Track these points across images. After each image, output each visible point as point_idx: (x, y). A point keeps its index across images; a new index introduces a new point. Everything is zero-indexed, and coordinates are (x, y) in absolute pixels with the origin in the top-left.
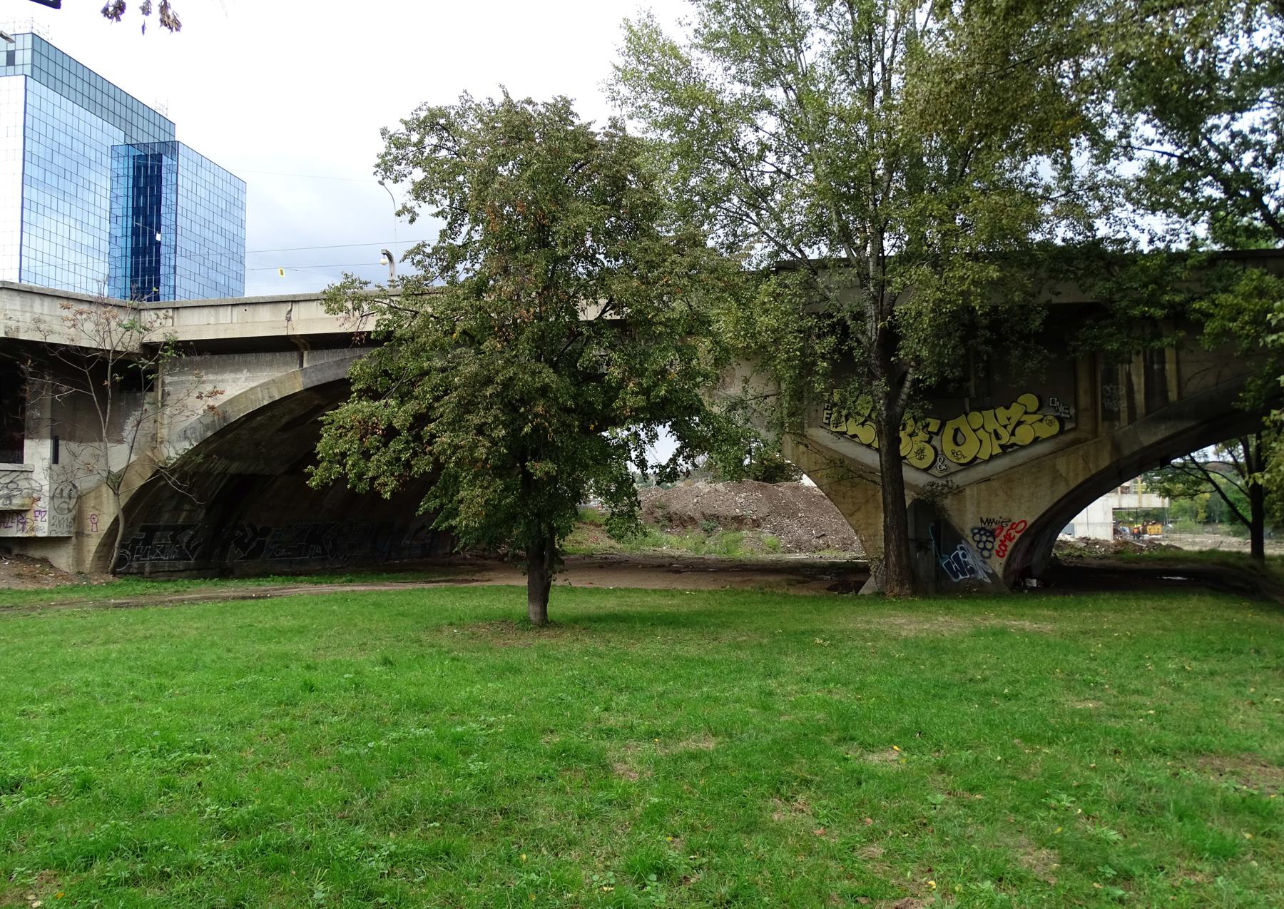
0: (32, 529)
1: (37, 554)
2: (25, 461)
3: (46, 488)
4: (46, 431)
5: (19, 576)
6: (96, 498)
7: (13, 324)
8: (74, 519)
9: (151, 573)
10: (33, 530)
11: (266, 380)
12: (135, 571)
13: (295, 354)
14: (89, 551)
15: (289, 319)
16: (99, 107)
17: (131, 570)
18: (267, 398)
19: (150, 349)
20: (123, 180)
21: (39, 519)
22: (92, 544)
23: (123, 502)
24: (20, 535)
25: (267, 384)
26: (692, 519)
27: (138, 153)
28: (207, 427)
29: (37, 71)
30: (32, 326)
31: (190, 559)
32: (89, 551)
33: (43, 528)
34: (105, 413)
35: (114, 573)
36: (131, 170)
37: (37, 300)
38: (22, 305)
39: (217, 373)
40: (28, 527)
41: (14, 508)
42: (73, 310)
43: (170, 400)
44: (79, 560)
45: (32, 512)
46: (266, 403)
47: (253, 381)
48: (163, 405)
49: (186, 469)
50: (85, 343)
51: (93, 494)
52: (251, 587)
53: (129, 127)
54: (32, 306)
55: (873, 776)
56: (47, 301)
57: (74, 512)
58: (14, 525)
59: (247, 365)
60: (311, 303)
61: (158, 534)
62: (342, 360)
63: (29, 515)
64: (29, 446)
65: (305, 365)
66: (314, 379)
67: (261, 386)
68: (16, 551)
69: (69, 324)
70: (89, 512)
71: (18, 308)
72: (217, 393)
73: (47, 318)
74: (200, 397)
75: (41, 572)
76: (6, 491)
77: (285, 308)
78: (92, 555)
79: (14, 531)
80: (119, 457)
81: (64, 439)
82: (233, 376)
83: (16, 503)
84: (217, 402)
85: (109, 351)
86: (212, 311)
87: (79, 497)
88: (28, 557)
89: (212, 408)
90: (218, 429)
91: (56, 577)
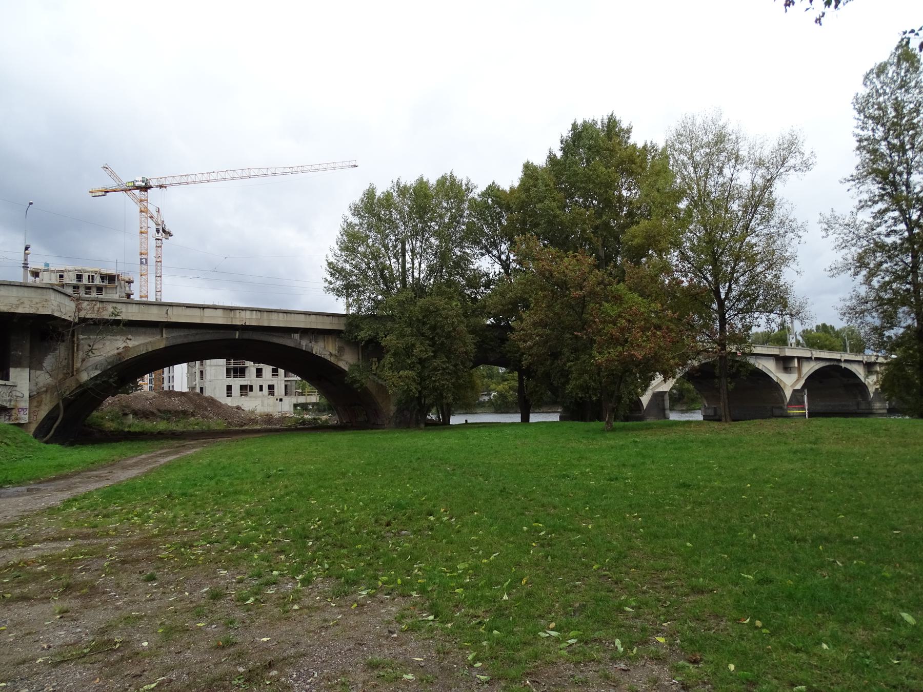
0: (17, 419)
15: (167, 313)
22: (33, 427)
25: (147, 343)
26: (153, 414)
28: (109, 363)
40: (13, 418)
63: (14, 411)
65: (164, 335)
77: (165, 308)
86: (137, 306)
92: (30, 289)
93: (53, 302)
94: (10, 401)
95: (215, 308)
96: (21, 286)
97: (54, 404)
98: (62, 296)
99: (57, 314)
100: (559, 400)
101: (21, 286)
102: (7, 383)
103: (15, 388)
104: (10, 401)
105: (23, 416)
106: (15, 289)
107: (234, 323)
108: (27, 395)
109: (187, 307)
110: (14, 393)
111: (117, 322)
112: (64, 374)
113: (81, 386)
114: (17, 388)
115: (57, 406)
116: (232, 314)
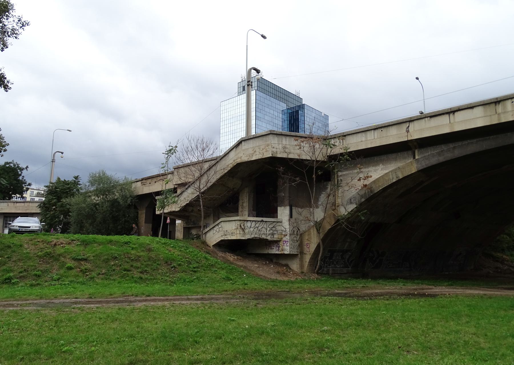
1: (284, 262)
3: (288, 230)
4: (287, 202)
5: (278, 272)
6: (308, 235)
7: (275, 150)
8: (299, 246)
9: (332, 274)
10: (283, 250)
11: (393, 168)
12: (326, 273)
13: (410, 152)
15: (408, 131)
16: (278, 97)
17: (324, 272)
18: (395, 178)
19: (333, 158)
20: (286, 122)
21: (285, 245)
22: (307, 258)
23: (322, 236)
24: (277, 252)
25: (396, 170)
27: (291, 111)
28: (362, 196)
29: (259, 88)
30: (282, 151)
31: (349, 268)
32: (306, 262)
33: (287, 249)
34: (312, 193)
35: (318, 273)
36: (288, 118)
37: (284, 138)
41: (275, 240)
42: (299, 141)
43: (343, 184)
44: (302, 266)
46: (394, 181)
47: (386, 170)
48: (338, 187)
49: (350, 219)
50: (304, 157)
51: (307, 233)
52: (410, 287)
53: (287, 103)
54: (282, 141)
55: (142, 256)
56: (288, 138)
57: (299, 242)
58: (275, 248)
59: (382, 162)
60: (421, 120)
61: (335, 254)
62: (442, 151)
63: (281, 243)
64: (280, 210)
65: (417, 157)
66: (424, 164)
67: (391, 171)
68: (274, 261)
69: (298, 147)
70: (306, 242)
71: (277, 142)
72: (368, 177)
73: (288, 146)
74: (359, 180)
75: (287, 271)
76: (271, 231)
78: (307, 263)
79: (274, 251)
80: (319, 214)
81: (294, 206)
82: (374, 168)
83: (276, 237)
84: (367, 182)
85: (314, 161)
86: (363, 134)
87: (301, 235)
88: (280, 264)
89: (365, 186)
90: (368, 197)
91: (293, 274)
94: (273, 234)
95: (471, 107)
98: (355, 136)
100: (251, 84)
103: (280, 224)
107: (503, 120)
109: (431, 117)
116: (500, 108)
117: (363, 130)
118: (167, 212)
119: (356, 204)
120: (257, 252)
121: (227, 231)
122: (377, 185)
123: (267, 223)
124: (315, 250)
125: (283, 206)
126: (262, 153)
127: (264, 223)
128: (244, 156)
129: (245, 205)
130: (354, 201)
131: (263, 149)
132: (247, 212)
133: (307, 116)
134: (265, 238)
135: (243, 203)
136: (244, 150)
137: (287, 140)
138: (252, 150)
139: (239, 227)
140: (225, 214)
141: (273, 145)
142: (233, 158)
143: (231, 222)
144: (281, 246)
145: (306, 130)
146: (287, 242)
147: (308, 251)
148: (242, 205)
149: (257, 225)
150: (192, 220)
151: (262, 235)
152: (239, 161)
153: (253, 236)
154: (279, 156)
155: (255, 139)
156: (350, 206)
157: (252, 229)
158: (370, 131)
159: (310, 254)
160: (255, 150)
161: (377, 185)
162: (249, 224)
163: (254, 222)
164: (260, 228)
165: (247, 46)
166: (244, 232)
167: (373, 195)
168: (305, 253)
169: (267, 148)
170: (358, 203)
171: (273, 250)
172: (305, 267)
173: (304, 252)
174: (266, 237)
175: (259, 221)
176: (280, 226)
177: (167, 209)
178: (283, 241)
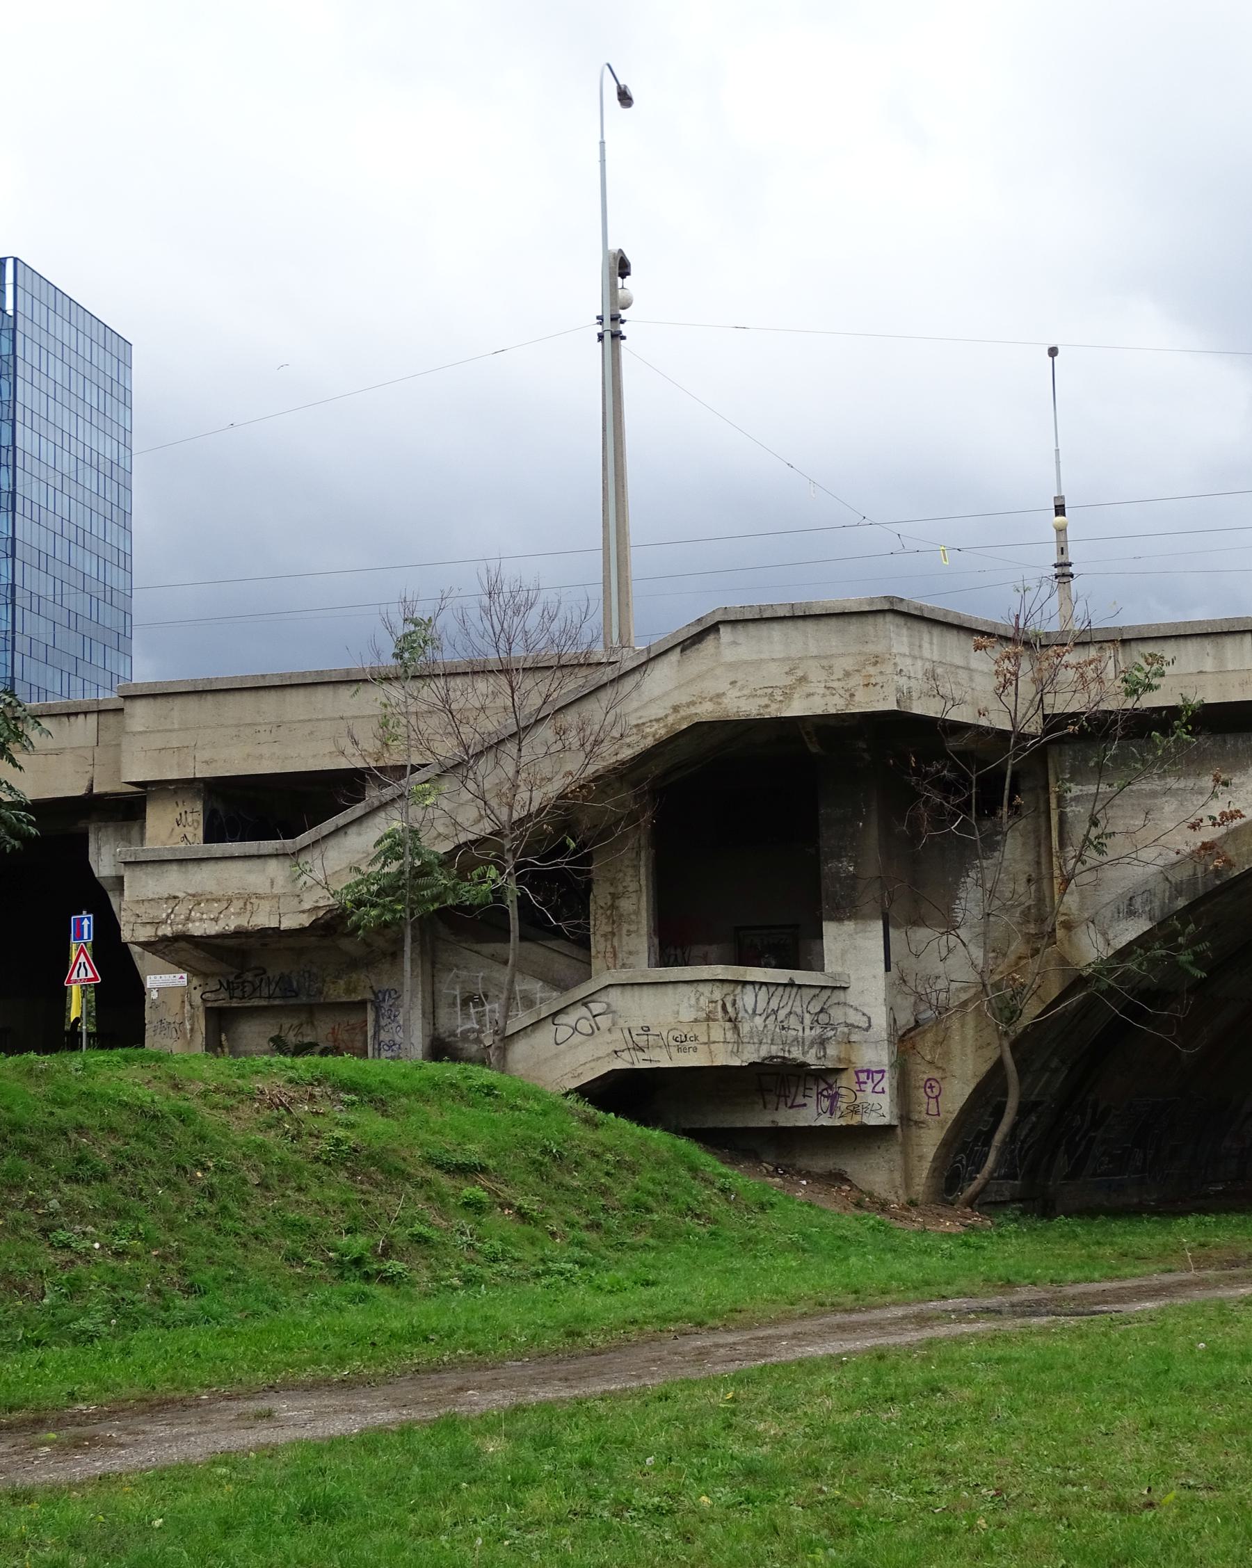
1: (821, 1164)
2: (828, 968)
10: (855, 1111)
14: (921, 1158)
21: (869, 1087)
22: (929, 1141)
24: (825, 1121)
28: (1178, 890)
32: (921, 1158)
38: (911, 645)
39: (1187, 775)
40: (842, 1105)
45: (851, 1072)
58: (811, 1102)
63: (845, 1081)
78: (927, 1165)
86: (1208, 645)
92: (823, 625)
93: (905, 664)
94: (822, 1042)
96: (793, 618)
97: (991, 1055)
98: (952, 638)
99: (919, 708)
101: (793, 618)
102: (800, 976)
104: (822, 1042)
105: (872, 1099)
106: (777, 631)
108: (880, 1020)
110: (837, 1014)
111: (1164, 719)
112: (1029, 938)
113: (1078, 982)
114: (851, 997)
115: (999, 1065)
117: (1210, 630)
118: (213, 933)
119: (1150, 919)
120: (710, 1124)
121: (647, 1029)
122: (1244, 849)
123: (804, 991)
124: (963, 1111)
125: (849, 918)
126: (842, 692)
127: (795, 990)
128: (733, 693)
129: (626, 905)
130: (1144, 904)
131: (847, 674)
132: (645, 939)
133: (28, 333)
134: (801, 1058)
135: (615, 897)
136: (732, 666)
137: (935, 641)
138: (787, 669)
139: (720, 1014)
140: (477, 947)
141: (898, 660)
142: (666, 694)
143: (670, 989)
144: (843, 1091)
145: (19, 417)
146: (877, 1077)
147: (933, 1111)
148: (613, 907)
149: (774, 1004)
150: (273, 972)
151: (791, 1045)
152: (706, 711)
153: (764, 1052)
154: (918, 708)
155: (800, 624)
156: (1123, 925)
157: (759, 1021)
158: (1238, 637)
159: (941, 1124)
160: (800, 673)
161: (1244, 849)
162: (748, 998)
163: (764, 989)
164: (782, 1014)
165: (602, 143)
166: (739, 1035)
167: (1221, 885)
168: (916, 1123)
169: (871, 670)
170: (1157, 913)
171: (803, 1111)
172: (917, 1180)
173: (915, 1117)
174: (804, 1053)
175: (778, 985)
176: (841, 1006)
177: (216, 920)
178: (857, 1073)
